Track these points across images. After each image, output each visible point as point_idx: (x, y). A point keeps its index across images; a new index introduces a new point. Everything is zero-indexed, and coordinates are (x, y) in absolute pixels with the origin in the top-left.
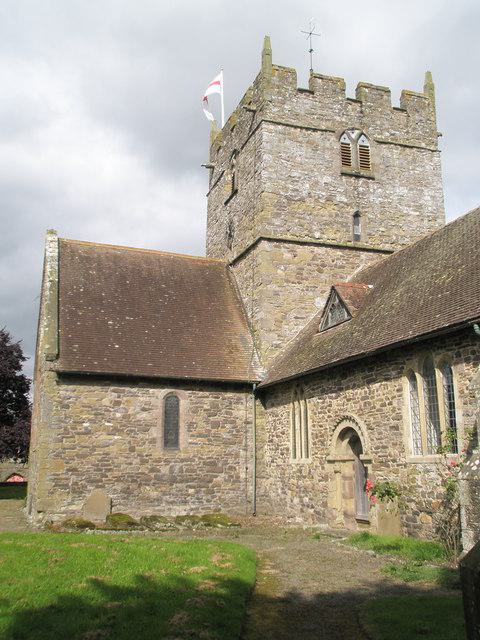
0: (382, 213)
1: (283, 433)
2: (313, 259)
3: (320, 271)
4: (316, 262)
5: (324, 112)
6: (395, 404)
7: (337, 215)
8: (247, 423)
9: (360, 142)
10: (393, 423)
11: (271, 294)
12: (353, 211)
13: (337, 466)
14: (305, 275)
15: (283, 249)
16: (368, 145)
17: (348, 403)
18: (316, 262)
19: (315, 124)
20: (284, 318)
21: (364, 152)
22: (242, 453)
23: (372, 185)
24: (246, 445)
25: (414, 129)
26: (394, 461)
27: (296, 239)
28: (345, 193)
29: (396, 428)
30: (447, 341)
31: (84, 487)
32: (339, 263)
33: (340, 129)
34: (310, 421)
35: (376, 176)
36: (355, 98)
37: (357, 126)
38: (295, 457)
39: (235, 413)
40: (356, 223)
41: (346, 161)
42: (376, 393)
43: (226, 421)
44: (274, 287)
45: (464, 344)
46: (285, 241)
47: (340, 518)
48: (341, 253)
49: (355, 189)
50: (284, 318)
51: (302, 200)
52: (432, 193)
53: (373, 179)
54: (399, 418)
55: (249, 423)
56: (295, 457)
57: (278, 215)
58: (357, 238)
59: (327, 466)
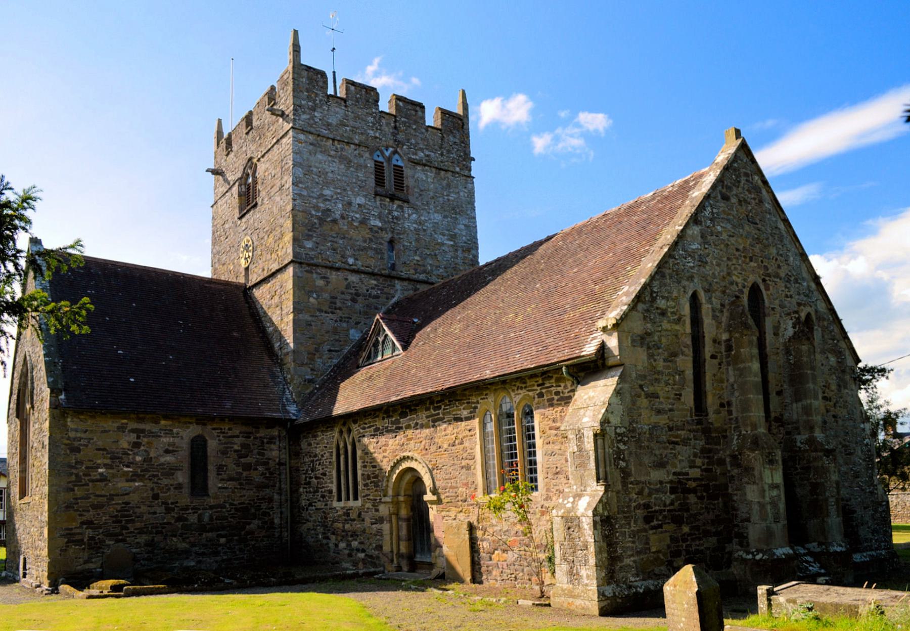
1: (324, 474)
10: (464, 463)
14: (339, 304)
15: (315, 276)
21: (399, 172)
28: (380, 217)
32: (374, 293)
34: (359, 464)
43: (258, 463)
49: (390, 212)
50: (317, 350)
56: (339, 499)
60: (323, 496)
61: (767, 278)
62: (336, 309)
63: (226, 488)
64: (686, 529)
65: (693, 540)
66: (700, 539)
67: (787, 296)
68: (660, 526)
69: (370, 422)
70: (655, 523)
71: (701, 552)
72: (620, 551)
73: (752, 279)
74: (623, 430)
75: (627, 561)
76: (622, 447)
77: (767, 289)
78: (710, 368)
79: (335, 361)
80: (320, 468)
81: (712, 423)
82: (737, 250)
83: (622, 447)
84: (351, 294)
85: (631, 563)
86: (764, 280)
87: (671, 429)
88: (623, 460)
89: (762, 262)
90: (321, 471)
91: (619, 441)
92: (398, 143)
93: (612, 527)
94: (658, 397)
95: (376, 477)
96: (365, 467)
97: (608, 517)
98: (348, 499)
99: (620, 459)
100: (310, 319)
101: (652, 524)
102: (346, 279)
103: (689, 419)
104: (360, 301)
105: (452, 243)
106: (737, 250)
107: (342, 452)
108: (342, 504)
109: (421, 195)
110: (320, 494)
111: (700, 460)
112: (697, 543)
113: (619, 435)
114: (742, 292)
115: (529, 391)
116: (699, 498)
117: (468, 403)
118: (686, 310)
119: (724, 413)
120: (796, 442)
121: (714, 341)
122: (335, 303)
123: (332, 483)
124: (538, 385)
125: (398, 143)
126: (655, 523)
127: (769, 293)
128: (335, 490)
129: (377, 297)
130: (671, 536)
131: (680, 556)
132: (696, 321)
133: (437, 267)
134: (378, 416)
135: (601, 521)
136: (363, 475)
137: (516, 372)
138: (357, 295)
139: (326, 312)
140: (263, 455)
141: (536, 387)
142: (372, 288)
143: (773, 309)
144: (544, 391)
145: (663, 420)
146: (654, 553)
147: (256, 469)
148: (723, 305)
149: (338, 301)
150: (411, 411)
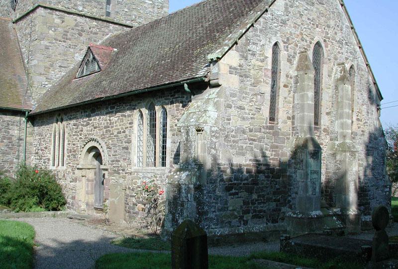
1: (46, 148)
2: (76, 25)
3: (80, 35)
4: (77, 28)
6: (127, 132)
10: (125, 145)
13: (83, 172)
14: (69, 36)
15: (54, 16)
17: (98, 124)
18: (77, 28)
20: (52, 65)
22: (15, 160)
27: (64, 9)
29: (127, 148)
32: (94, 30)
42: (115, 125)
44: (46, 43)
46: (56, 10)
47: (83, 207)
48: (96, 24)
50: (52, 65)
54: (129, 142)
58: (108, 14)
59: (77, 171)
60: (45, 163)
61: (327, 40)
62: (67, 39)
64: (255, 196)
65: (259, 203)
66: (264, 203)
67: (339, 52)
68: (237, 194)
69: (74, 115)
70: (234, 191)
71: (264, 212)
73: (316, 39)
74: (216, 128)
75: (211, 215)
77: (326, 46)
78: (283, 93)
79: (63, 74)
81: (280, 129)
82: (309, 19)
83: (214, 140)
84: (78, 30)
85: (213, 216)
86: (325, 41)
87: (251, 131)
88: (215, 149)
89: (324, 29)
91: (212, 136)
93: (202, 191)
94: (244, 109)
95: (74, 151)
96: (69, 144)
99: (212, 148)
100: (48, 44)
101: (231, 192)
102: (76, 20)
103: (264, 125)
105: (151, 2)
106: (309, 19)
107: (57, 134)
110: (43, 160)
111: (270, 153)
112: (262, 205)
113: (213, 132)
114: (310, 47)
115: (165, 99)
116: (266, 177)
117: (130, 105)
118: (269, 53)
119: (289, 122)
121: (287, 76)
122: (67, 35)
123: (50, 153)
124: (171, 96)
126: (234, 191)
127: (328, 49)
128: (51, 159)
129: (96, 33)
130: (244, 201)
131: (249, 213)
132: (275, 61)
133: (139, 17)
134: (78, 111)
136: (68, 149)
137: (158, 86)
138: (83, 31)
139: (60, 41)
140: (9, 133)
141: (170, 97)
142: (93, 27)
143: (329, 59)
144: (174, 100)
145: (246, 125)
146: (231, 211)
148: (295, 53)
149: (68, 34)
150: (98, 108)
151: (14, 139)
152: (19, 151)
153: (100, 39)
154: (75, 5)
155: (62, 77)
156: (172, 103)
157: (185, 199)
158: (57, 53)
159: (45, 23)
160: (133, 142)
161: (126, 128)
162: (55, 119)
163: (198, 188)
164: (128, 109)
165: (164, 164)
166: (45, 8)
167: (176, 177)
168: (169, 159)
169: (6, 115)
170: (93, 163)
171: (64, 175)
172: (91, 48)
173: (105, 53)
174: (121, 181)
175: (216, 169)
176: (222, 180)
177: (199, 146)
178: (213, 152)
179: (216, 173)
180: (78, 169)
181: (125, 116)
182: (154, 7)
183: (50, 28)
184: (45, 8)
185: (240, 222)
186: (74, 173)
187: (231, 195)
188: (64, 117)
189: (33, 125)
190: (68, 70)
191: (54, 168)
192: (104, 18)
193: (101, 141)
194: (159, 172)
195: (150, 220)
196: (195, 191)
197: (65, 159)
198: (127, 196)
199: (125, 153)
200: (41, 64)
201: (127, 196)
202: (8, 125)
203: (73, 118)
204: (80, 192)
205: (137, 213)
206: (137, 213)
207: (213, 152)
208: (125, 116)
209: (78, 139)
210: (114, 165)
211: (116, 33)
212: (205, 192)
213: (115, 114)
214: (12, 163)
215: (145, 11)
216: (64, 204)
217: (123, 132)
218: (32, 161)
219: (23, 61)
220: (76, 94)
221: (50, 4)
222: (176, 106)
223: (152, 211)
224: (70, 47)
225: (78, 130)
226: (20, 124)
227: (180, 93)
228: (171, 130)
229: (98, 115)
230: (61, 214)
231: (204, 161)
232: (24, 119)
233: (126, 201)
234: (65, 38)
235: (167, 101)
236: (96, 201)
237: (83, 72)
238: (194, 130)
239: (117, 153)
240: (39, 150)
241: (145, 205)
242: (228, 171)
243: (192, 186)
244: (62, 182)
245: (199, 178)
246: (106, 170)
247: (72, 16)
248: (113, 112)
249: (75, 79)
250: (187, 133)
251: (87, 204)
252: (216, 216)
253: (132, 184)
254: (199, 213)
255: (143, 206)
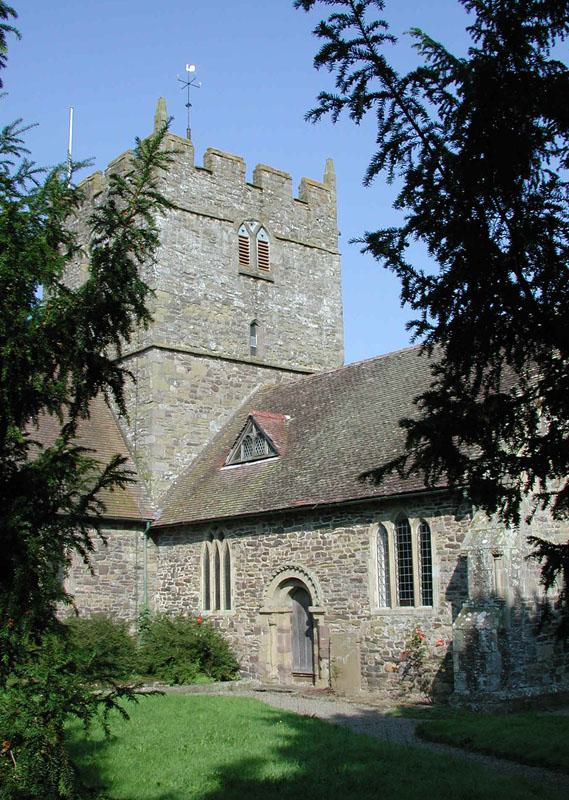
0: (281, 323)
1: (188, 581)
2: (208, 375)
3: (215, 390)
4: (211, 379)
5: (223, 197)
6: (358, 556)
7: (234, 323)
8: (138, 568)
9: (259, 237)
10: (355, 575)
11: (163, 415)
12: (251, 319)
13: (274, 618)
14: (199, 393)
15: (176, 362)
16: (267, 241)
17: (298, 547)
18: (211, 379)
19: (212, 211)
20: (176, 443)
21: (263, 247)
22: (132, 602)
23: (272, 290)
24: (136, 594)
25: (315, 226)
26: (354, 613)
27: (189, 349)
28: (243, 298)
29: (360, 581)
30: (426, 500)
31: (246, 725)
32: (235, 380)
33: (240, 220)
34: (233, 572)
35: (274, 277)
36: (203, 167)
37: (257, 217)
38: (208, 607)
39: (125, 556)
40: (253, 334)
41: (244, 259)
42: (333, 545)
43: (115, 566)
44: (165, 406)
45: (445, 505)
46: (178, 351)
47: (274, 672)
48: (237, 369)
49: (254, 292)
50: (176, 443)
51: (198, 303)
52: (331, 303)
53: (272, 282)
54: (364, 570)
55: (139, 568)
56: (208, 607)
57: (172, 319)
58: (253, 351)
59: (259, 618)
63: (83, 592)
69: (247, 529)
70: (542, 635)
72: (512, 660)
75: (518, 670)
76: (516, 567)
79: (194, 455)
80: (183, 573)
83: (516, 567)
85: (521, 671)
90: (185, 577)
91: (513, 562)
92: (264, 217)
93: (506, 637)
94: (546, 520)
97: (504, 630)
98: (218, 607)
100: (169, 409)
102: (208, 366)
104: (220, 389)
105: (316, 326)
108: (209, 613)
109: (286, 273)
120: (544, 606)
122: (195, 392)
124: (436, 505)
125: (264, 217)
126: (542, 635)
135: (498, 633)
136: (237, 583)
140: (121, 557)
147: (113, 573)
151: (129, 567)
152: (136, 586)
153: (246, 394)
154: (205, 341)
155: (193, 462)
156: (438, 514)
157: (486, 649)
158: (183, 424)
159: (162, 374)
160: (370, 571)
161: (355, 551)
162: (206, 534)
163: (502, 633)
164: (357, 523)
165: (428, 600)
166: (161, 348)
167: (469, 619)
168: (438, 594)
169: (116, 529)
170: (288, 603)
171: (232, 623)
172: (255, 418)
173: (276, 425)
174: (351, 629)
175: (519, 606)
176: (528, 621)
177: (499, 577)
178: (516, 583)
179: (518, 611)
180: (261, 613)
181: (353, 532)
182: (321, 334)
183: (170, 381)
184: (161, 348)
185: (552, 677)
186: (253, 621)
187: (539, 640)
188: (226, 531)
189: (157, 543)
190: (200, 449)
191: (209, 613)
192: (248, 358)
193: (307, 570)
194: (422, 614)
195: (408, 684)
196: (499, 637)
197: (232, 598)
198: (363, 651)
199: (356, 587)
200: (161, 442)
201: (363, 651)
202: (120, 544)
203: (246, 534)
204: (267, 646)
205: (384, 676)
206: (384, 676)
207: (516, 583)
208: (353, 532)
209: (259, 566)
210: (336, 606)
211: (267, 383)
212: (510, 638)
213: (334, 529)
214: (127, 606)
215: (308, 341)
216: (236, 669)
217: (350, 556)
218: (159, 604)
219: (124, 436)
220: (248, 496)
221: (168, 342)
222: (446, 519)
223: (412, 671)
224: (201, 411)
225: (258, 552)
226: (137, 542)
227: (451, 500)
228: (439, 553)
229: (298, 530)
230: (240, 686)
231: (506, 596)
232: (142, 534)
233: (363, 659)
234: (194, 398)
235: (428, 512)
236: (295, 661)
237: (238, 456)
238: (490, 555)
239: (341, 588)
240: (170, 584)
241: (397, 663)
242: (534, 607)
243: (494, 631)
244: (229, 636)
245: (502, 620)
246: (322, 613)
247: (201, 359)
248: (328, 526)
249: (224, 466)
250: (479, 559)
251: (281, 668)
252: (524, 670)
253: (371, 633)
254: (505, 667)
255: (394, 665)
